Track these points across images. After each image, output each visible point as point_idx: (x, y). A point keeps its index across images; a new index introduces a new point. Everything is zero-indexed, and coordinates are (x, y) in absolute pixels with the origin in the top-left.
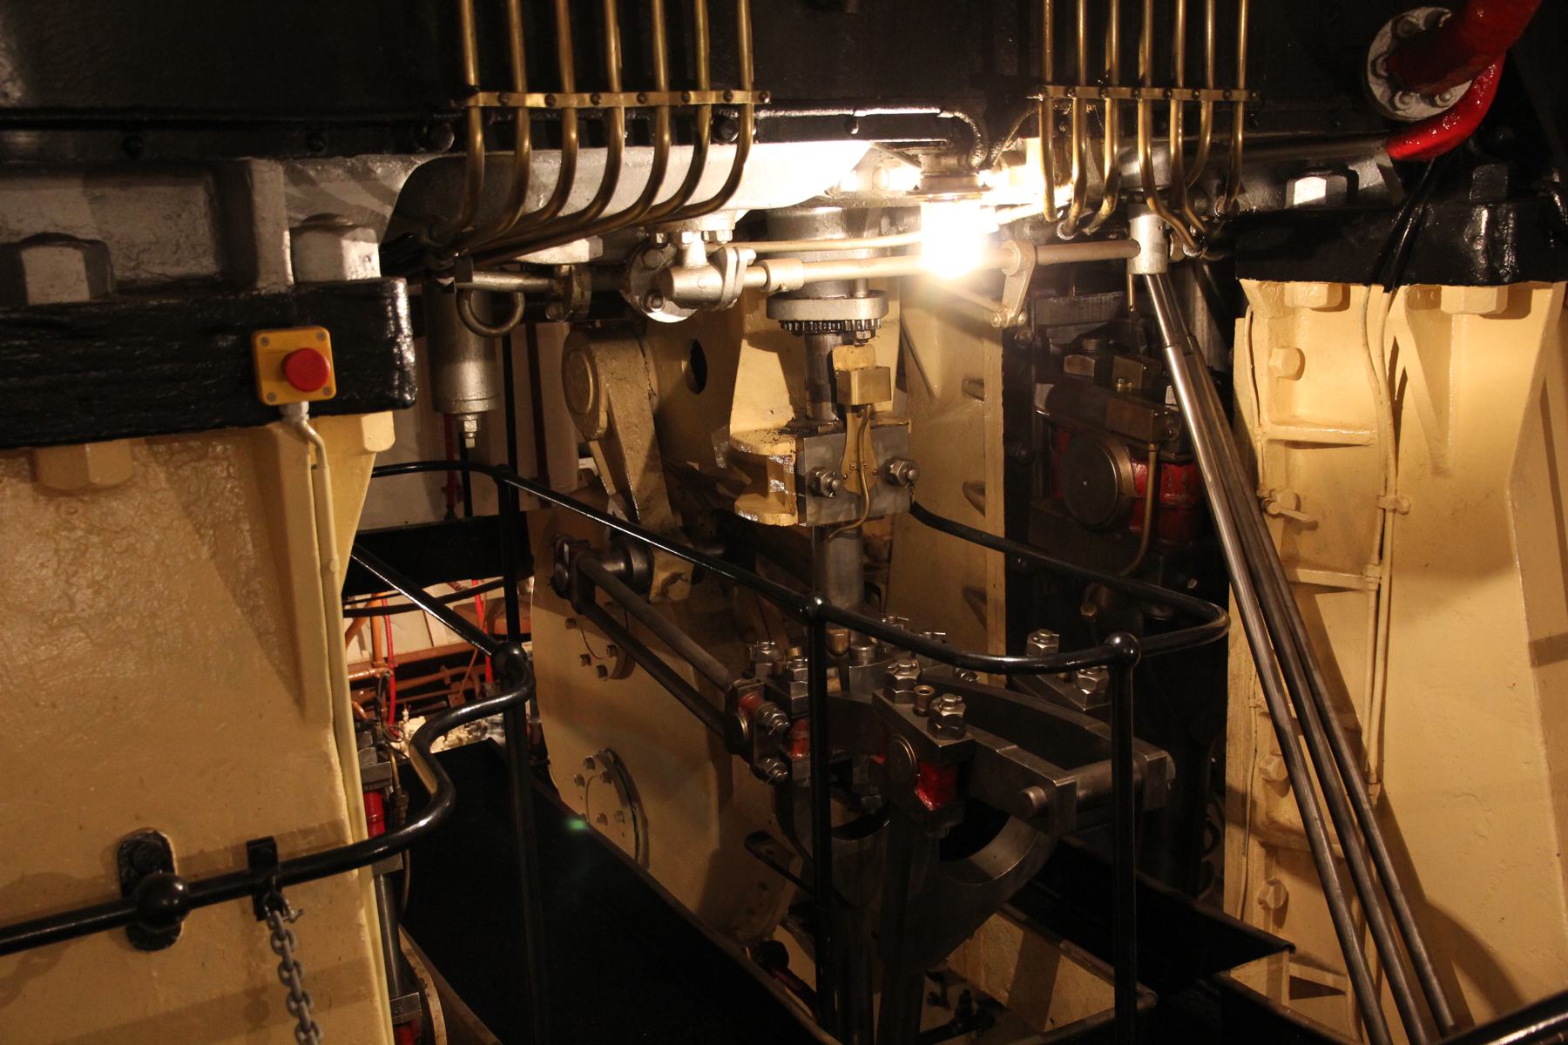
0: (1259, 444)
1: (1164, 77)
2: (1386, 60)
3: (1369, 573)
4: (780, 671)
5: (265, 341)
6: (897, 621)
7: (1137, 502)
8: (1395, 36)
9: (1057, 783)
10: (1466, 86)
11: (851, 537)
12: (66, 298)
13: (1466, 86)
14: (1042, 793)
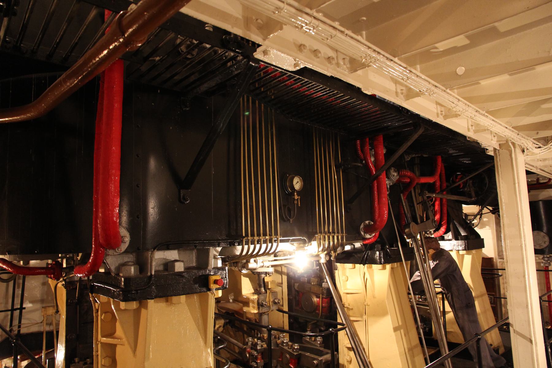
0: (341, 294)
1: (334, 232)
2: (363, 229)
3: (364, 317)
4: (254, 343)
5: (212, 278)
6: (274, 333)
7: (318, 306)
8: (364, 225)
9: (320, 359)
10: (374, 234)
11: (267, 315)
12: (180, 271)
13: (374, 234)
14: (317, 361)
